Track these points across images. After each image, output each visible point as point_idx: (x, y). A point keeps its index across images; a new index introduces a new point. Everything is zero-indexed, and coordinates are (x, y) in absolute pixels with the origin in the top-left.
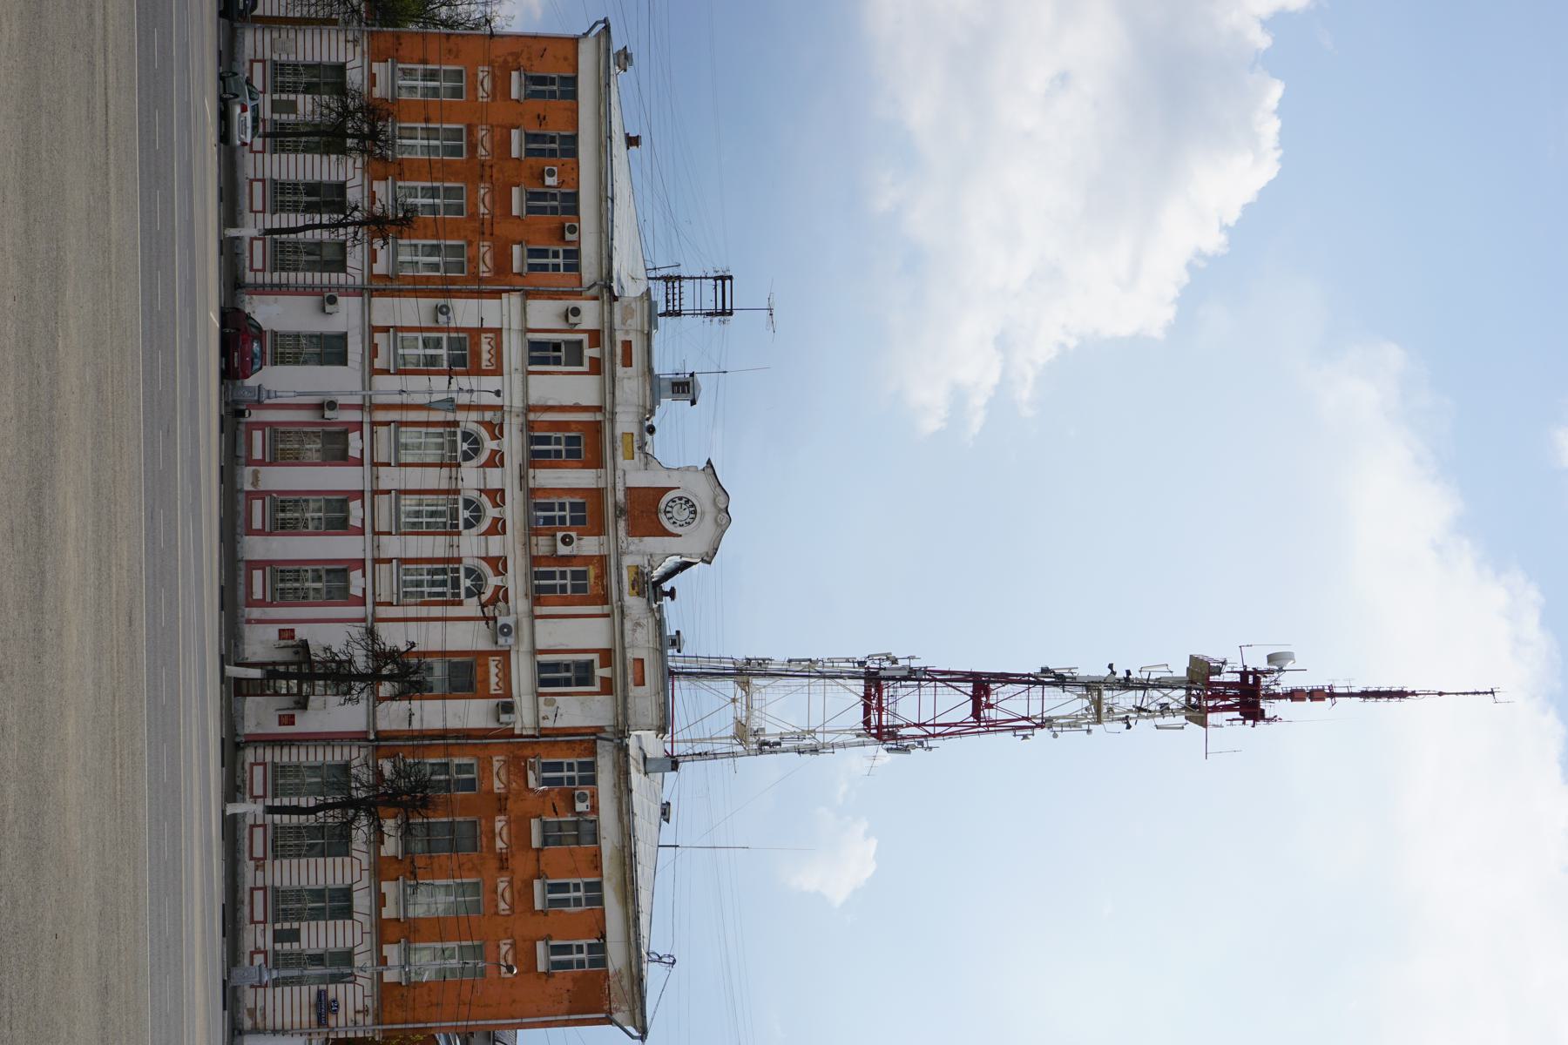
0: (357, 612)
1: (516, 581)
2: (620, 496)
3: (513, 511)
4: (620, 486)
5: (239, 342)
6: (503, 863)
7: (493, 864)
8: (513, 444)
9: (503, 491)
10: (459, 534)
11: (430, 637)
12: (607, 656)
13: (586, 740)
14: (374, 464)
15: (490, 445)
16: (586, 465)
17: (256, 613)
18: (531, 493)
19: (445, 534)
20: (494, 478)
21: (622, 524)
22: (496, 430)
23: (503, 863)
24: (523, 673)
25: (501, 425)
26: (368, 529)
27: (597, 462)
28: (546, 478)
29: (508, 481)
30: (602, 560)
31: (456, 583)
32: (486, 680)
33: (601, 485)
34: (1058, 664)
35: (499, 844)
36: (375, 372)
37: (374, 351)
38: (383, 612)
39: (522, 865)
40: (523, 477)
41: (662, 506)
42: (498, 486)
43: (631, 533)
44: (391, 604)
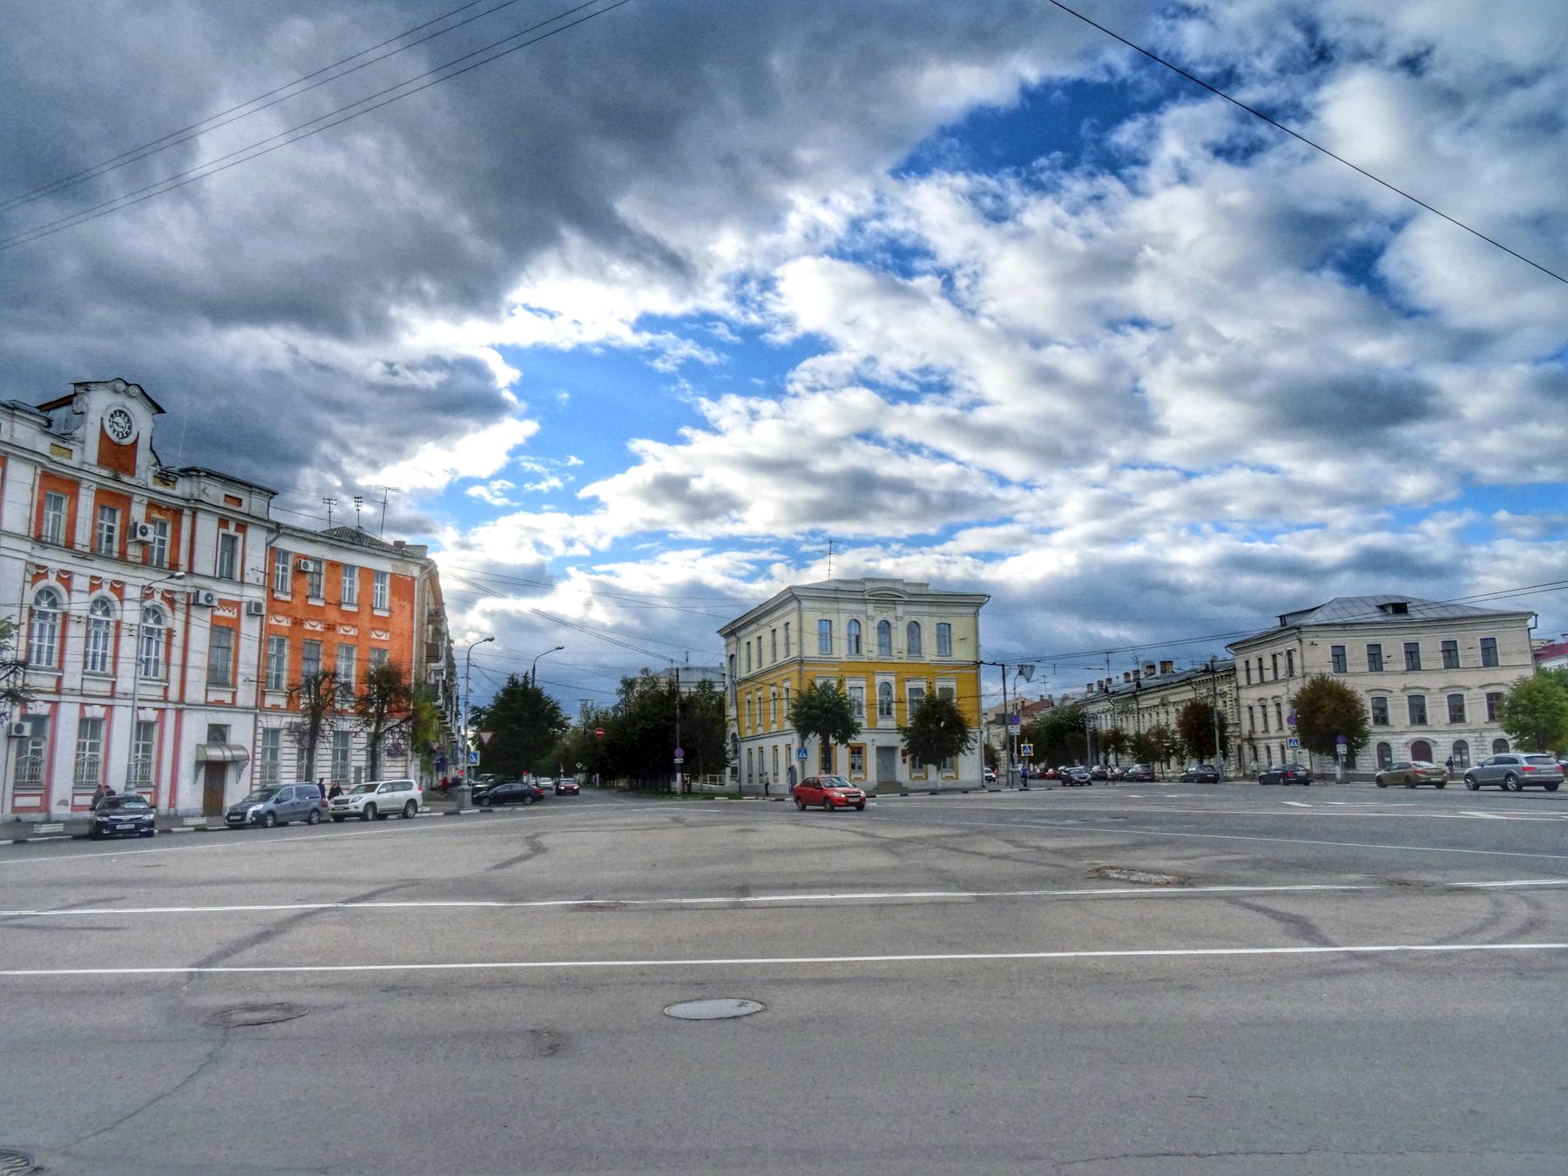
0: (170, 717)
1: (161, 583)
2: (105, 473)
3: (109, 572)
4: (97, 470)
5: (107, 824)
6: (331, 628)
7: (330, 634)
8: (56, 560)
9: (93, 577)
10: (118, 624)
11: (199, 658)
12: (223, 522)
13: (274, 554)
14: (58, 691)
15: (52, 581)
16: (75, 496)
17: (164, 801)
18: (94, 553)
19: (117, 637)
20: (80, 582)
21: (126, 479)
22: (40, 573)
23: (297, 623)
24: (224, 591)
25: (38, 567)
26: (109, 702)
27: (73, 486)
28: (83, 537)
29: (83, 571)
30: (152, 505)
31: (98, 622)
32: (227, 619)
33: (94, 487)
34: (545, 306)
35: (319, 628)
36: (233, 704)
37: (219, 703)
38: (174, 694)
39: (333, 615)
40: (84, 556)
41: (115, 439)
42: (87, 580)
43: (132, 473)
44: (166, 688)
